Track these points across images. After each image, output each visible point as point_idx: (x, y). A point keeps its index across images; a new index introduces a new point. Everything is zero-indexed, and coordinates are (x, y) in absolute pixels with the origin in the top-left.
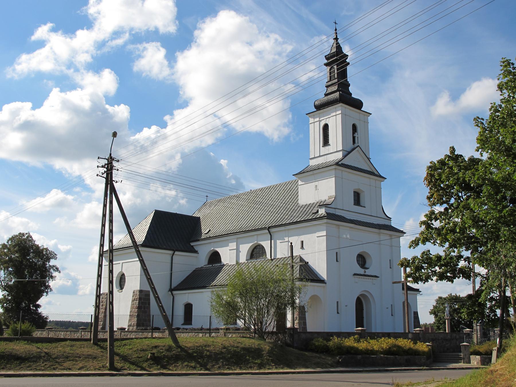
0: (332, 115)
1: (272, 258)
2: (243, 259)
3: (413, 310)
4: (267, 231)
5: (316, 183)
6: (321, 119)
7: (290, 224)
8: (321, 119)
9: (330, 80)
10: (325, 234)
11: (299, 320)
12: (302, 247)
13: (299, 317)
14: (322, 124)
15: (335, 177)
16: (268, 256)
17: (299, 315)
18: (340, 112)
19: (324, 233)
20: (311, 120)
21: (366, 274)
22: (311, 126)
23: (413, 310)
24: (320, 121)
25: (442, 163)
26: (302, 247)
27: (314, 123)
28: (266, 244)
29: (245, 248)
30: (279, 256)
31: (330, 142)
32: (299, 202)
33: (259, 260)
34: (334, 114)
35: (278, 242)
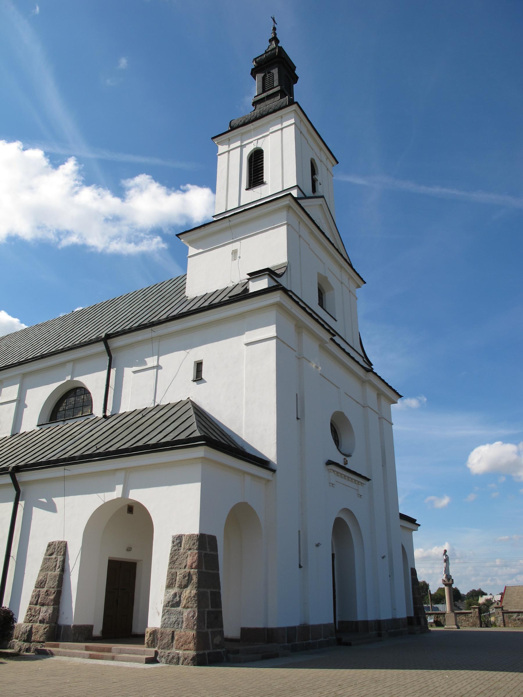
0: (271, 131)
1: (108, 414)
2: (30, 423)
3: (410, 567)
4: (101, 347)
5: (236, 246)
6: (245, 143)
7: (169, 319)
8: (245, 143)
9: (264, 91)
10: (274, 334)
11: (199, 585)
12: (198, 377)
13: (200, 574)
14: (248, 150)
15: (288, 224)
16: (98, 411)
17: (198, 567)
18: (292, 121)
19: (271, 331)
20: (222, 149)
21: (347, 466)
22: (222, 161)
23: (410, 567)
24: (242, 147)
25: (30, 609)
26: (198, 377)
27: (229, 151)
28: (94, 382)
29: (39, 396)
30: (126, 407)
31: (267, 177)
32: (186, 294)
33: (70, 422)
34: (279, 127)
35: (128, 371)
